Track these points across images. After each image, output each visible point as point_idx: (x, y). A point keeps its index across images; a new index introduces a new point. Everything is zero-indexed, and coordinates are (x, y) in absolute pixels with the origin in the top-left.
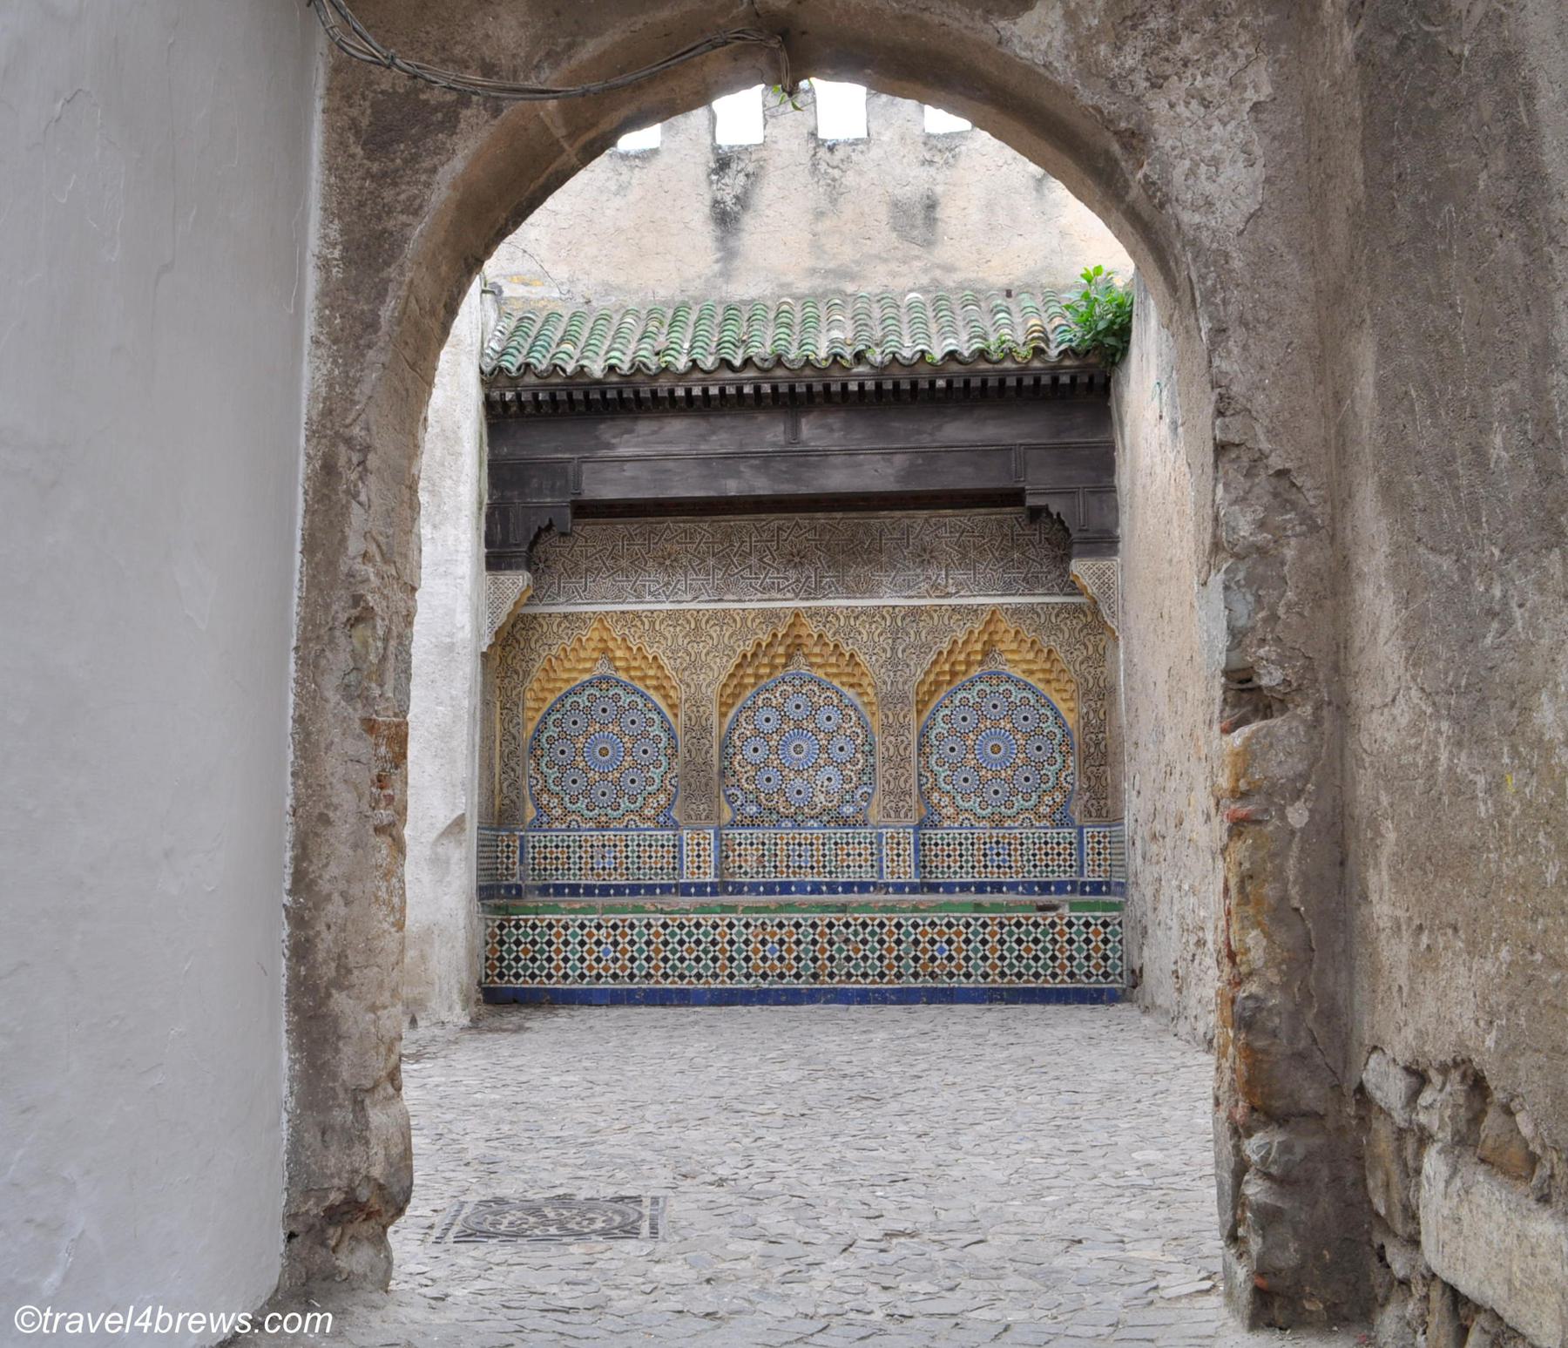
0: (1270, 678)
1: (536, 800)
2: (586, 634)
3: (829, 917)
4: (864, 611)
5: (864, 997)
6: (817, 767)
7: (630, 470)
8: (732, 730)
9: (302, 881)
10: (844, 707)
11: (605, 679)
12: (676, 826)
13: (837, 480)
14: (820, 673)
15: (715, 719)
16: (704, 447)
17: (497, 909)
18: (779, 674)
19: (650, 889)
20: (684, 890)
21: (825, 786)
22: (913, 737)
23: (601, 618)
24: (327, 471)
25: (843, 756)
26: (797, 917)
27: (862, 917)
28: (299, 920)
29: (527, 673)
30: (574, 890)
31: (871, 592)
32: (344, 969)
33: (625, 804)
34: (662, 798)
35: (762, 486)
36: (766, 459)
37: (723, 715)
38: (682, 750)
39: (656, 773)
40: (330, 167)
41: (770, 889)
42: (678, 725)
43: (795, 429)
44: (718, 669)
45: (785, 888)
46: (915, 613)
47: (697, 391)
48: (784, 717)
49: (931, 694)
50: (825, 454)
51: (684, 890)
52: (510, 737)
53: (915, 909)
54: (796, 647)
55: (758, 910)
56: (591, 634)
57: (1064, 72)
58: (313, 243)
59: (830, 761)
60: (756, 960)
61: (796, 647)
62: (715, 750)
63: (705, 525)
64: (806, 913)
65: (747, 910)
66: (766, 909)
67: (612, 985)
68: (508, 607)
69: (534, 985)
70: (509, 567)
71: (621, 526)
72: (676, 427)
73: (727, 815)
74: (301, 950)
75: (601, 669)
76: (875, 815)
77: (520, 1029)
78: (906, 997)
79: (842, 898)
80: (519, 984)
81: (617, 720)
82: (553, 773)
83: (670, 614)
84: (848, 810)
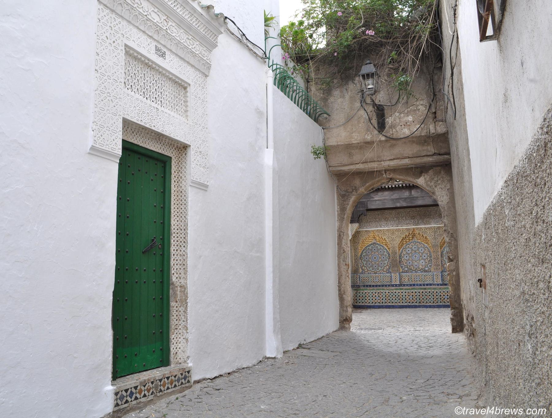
0: (451, 257)
1: (362, 268)
2: (370, 234)
3: (422, 291)
4: (428, 228)
5: (430, 307)
6: (420, 260)
7: (377, 202)
8: (401, 253)
9: (339, 282)
10: (425, 248)
11: (374, 243)
12: (391, 273)
13: (420, 202)
14: (419, 241)
15: (398, 251)
16: (392, 197)
17: (355, 290)
18: (411, 241)
19: (386, 286)
20: (393, 286)
21: (422, 264)
22: (440, 254)
23: (373, 231)
24: (339, 236)
25: (425, 258)
26: (416, 291)
27: (429, 290)
28: (339, 287)
29: (359, 243)
30: (370, 286)
31: (429, 224)
32: (344, 292)
33: (380, 268)
34: (387, 267)
35: (404, 204)
36: (405, 199)
37: (399, 250)
38: (391, 257)
39: (386, 262)
40: (338, 200)
41: (411, 285)
42: (390, 252)
43: (411, 193)
44: (398, 241)
45: (414, 285)
46: (439, 228)
47: (390, 186)
48: (412, 250)
49: (443, 244)
50: (417, 197)
51: (393, 286)
52: (356, 256)
53: (440, 289)
54: (414, 236)
55: (408, 289)
56: (371, 234)
57: (424, 185)
58: (336, 209)
59: (422, 259)
60: (408, 299)
61: (414, 236)
62: (398, 257)
63: (394, 211)
64: (417, 291)
65: (405, 289)
66: (409, 289)
67: (379, 304)
68: (355, 230)
69: (363, 304)
70: (354, 222)
71: (376, 212)
72: (386, 193)
73: (401, 270)
74: (340, 290)
75: (374, 241)
76: (432, 270)
77: (361, 312)
78: (439, 307)
79: (426, 287)
80: (360, 304)
81: (377, 251)
82: (365, 263)
83: (387, 230)
84: (426, 269)
